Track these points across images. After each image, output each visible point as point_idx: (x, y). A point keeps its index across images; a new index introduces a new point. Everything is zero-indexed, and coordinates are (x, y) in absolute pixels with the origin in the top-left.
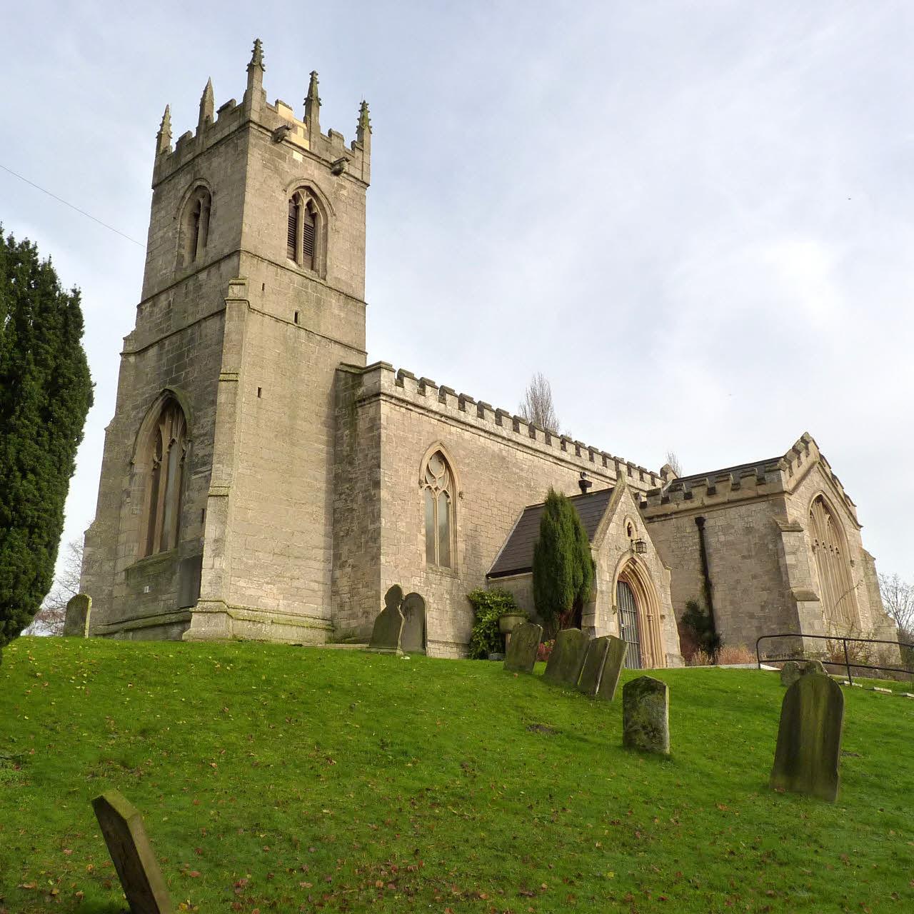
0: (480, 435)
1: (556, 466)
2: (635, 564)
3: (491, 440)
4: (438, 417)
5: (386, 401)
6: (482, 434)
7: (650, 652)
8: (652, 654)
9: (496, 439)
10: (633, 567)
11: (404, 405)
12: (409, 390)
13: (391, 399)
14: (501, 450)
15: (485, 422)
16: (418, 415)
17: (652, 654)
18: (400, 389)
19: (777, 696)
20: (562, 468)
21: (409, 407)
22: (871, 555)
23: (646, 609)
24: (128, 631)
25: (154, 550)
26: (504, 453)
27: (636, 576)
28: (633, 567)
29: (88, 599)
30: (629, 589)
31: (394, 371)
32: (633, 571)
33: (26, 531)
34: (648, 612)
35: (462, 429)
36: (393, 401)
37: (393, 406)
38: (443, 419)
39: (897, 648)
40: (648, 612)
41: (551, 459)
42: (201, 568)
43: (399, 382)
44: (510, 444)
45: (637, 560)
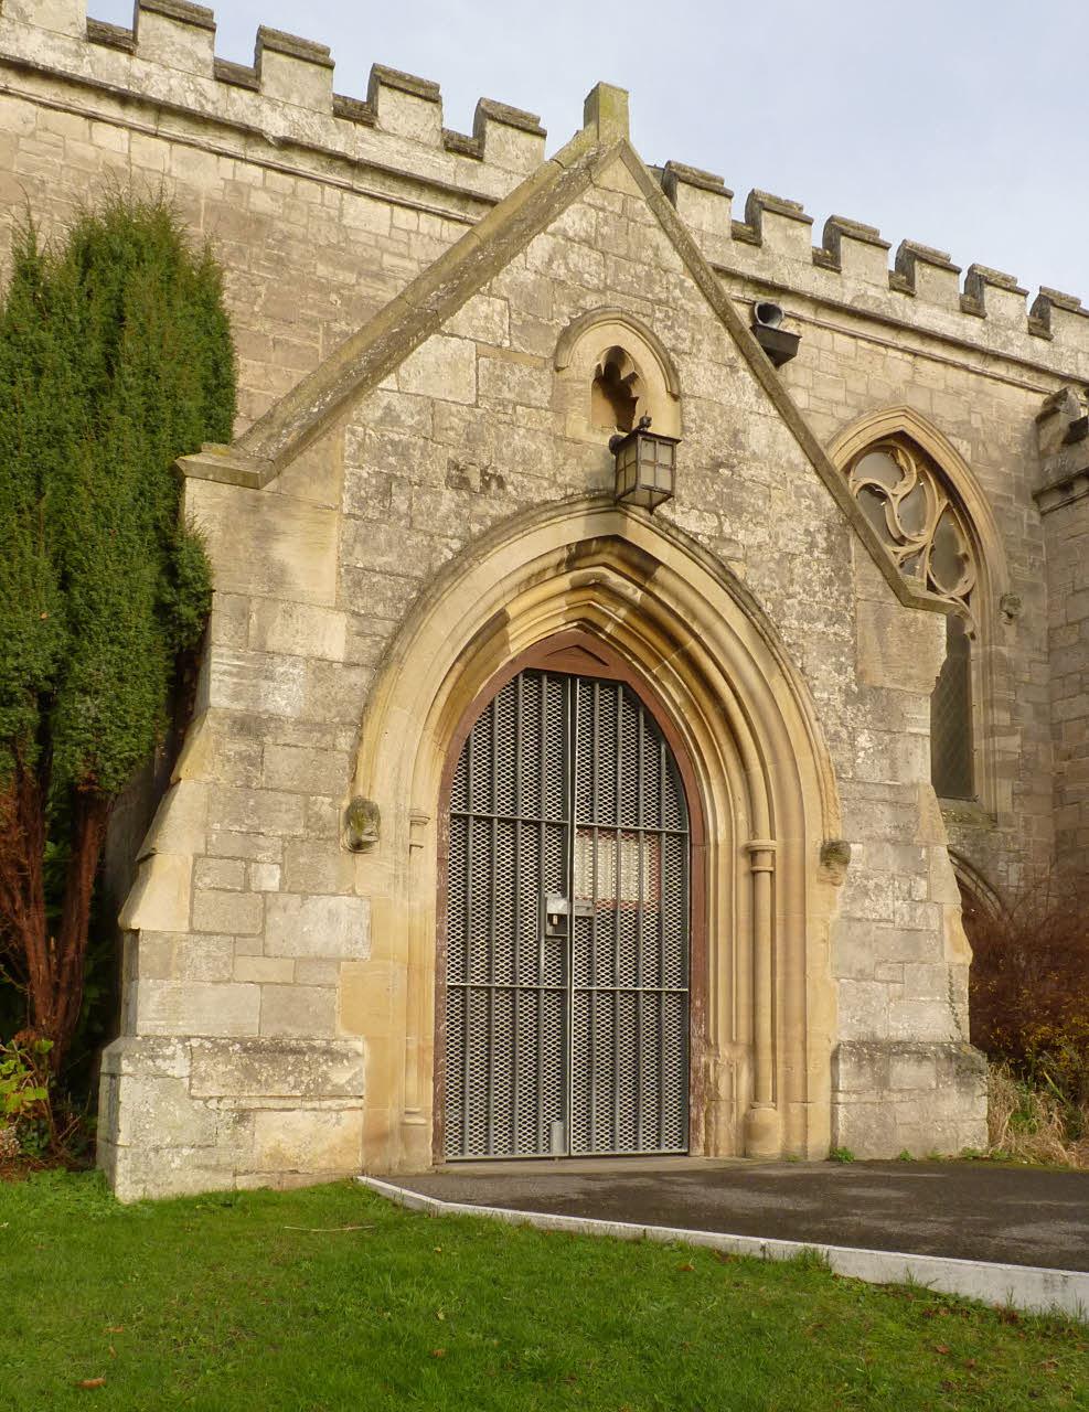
0: (92, 118)
2: (648, 575)
3: (172, 141)
7: (744, 1037)
8: (753, 1048)
9: (206, 138)
10: (638, 596)
12: (865, 278)
13: (158, 121)
14: (237, 188)
15: (138, 67)
17: (753, 1048)
18: (1039, 343)
22: (568, 141)
23: (742, 816)
26: (261, 202)
27: (675, 643)
28: (638, 596)
30: (649, 717)
31: (957, 272)
32: (639, 611)
34: (753, 830)
35: (267, 167)
40: (753, 830)
43: (1040, 325)
44: (304, 164)
45: (660, 549)
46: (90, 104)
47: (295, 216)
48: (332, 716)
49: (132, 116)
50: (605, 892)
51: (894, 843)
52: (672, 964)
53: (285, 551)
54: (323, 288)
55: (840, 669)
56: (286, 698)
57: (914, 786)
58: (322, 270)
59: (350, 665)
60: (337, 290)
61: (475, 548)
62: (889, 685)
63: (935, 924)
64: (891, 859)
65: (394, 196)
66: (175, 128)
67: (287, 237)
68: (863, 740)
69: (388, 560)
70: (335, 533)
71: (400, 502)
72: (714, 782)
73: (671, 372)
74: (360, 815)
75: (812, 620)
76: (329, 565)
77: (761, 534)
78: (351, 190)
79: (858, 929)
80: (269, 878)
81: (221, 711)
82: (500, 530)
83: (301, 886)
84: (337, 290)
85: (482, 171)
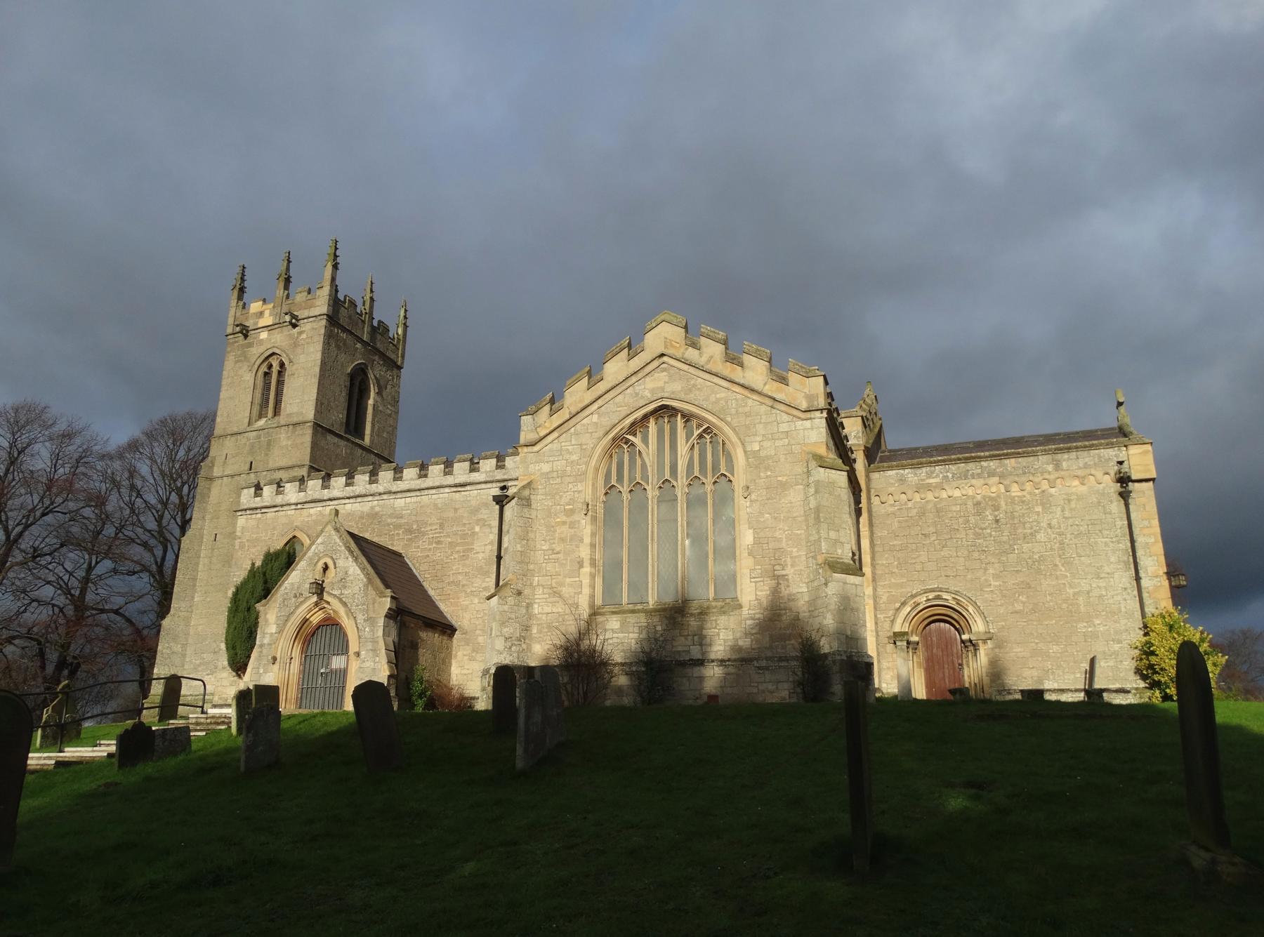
0: (345, 504)
1: (458, 494)
4: (293, 507)
5: (241, 515)
6: (347, 501)
9: (366, 499)
11: (258, 511)
16: (274, 514)
19: (822, 402)
20: (468, 493)
21: (263, 511)
24: (267, 374)
25: (973, 608)
26: (377, 509)
29: (881, 456)
33: (694, 389)
36: (248, 512)
37: (249, 516)
38: (299, 506)
39: (32, 506)
41: (447, 490)
42: (1165, 555)
46: (343, 501)
47: (384, 510)
48: (272, 642)
49: (351, 501)
50: (338, 667)
51: (372, 650)
52: (341, 682)
53: (268, 616)
54: (389, 525)
55: (363, 615)
56: (266, 641)
57: (378, 637)
58: (389, 520)
59: (276, 633)
60: (392, 524)
61: (297, 607)
62: (374, 616)
63: (379, 667)
64: (371, 654)
65: (625, 387)
66: (359, 500)
67: (382, 515)
68: (367, 629)
69: (283, 614)
70: (276, 610)
71: (286, 603)
72: (971, 609)
73: (335, 564)
74: (275, 659)
75: (358, 606)
76: (274, 616)
77: (350, 591)
78: (395, 498)
79: (361, 670)
80: (261, 671)
81: (1151, 588)
82: (302, 603)
83: (265, 672)
84: (392, 524)
85: (427, 480)
